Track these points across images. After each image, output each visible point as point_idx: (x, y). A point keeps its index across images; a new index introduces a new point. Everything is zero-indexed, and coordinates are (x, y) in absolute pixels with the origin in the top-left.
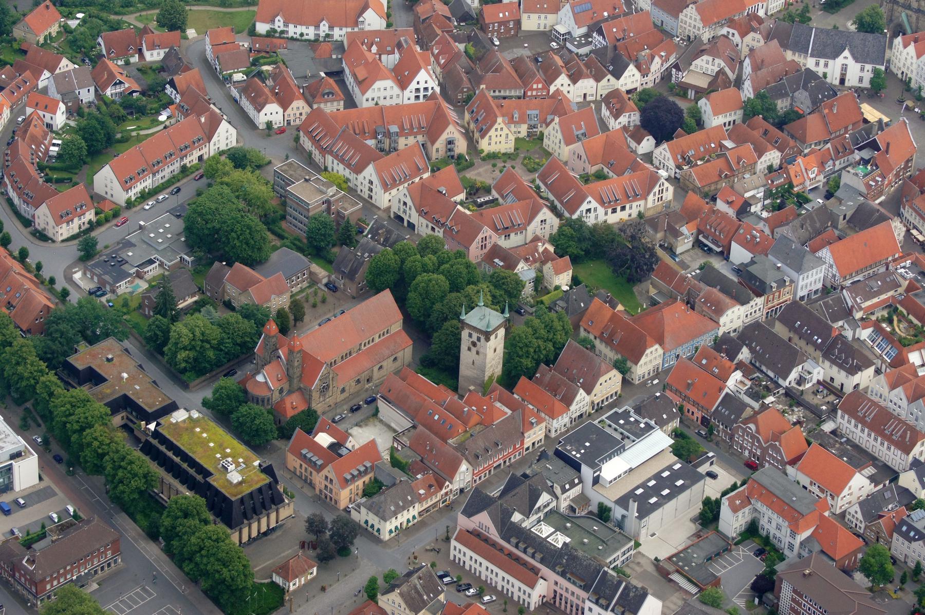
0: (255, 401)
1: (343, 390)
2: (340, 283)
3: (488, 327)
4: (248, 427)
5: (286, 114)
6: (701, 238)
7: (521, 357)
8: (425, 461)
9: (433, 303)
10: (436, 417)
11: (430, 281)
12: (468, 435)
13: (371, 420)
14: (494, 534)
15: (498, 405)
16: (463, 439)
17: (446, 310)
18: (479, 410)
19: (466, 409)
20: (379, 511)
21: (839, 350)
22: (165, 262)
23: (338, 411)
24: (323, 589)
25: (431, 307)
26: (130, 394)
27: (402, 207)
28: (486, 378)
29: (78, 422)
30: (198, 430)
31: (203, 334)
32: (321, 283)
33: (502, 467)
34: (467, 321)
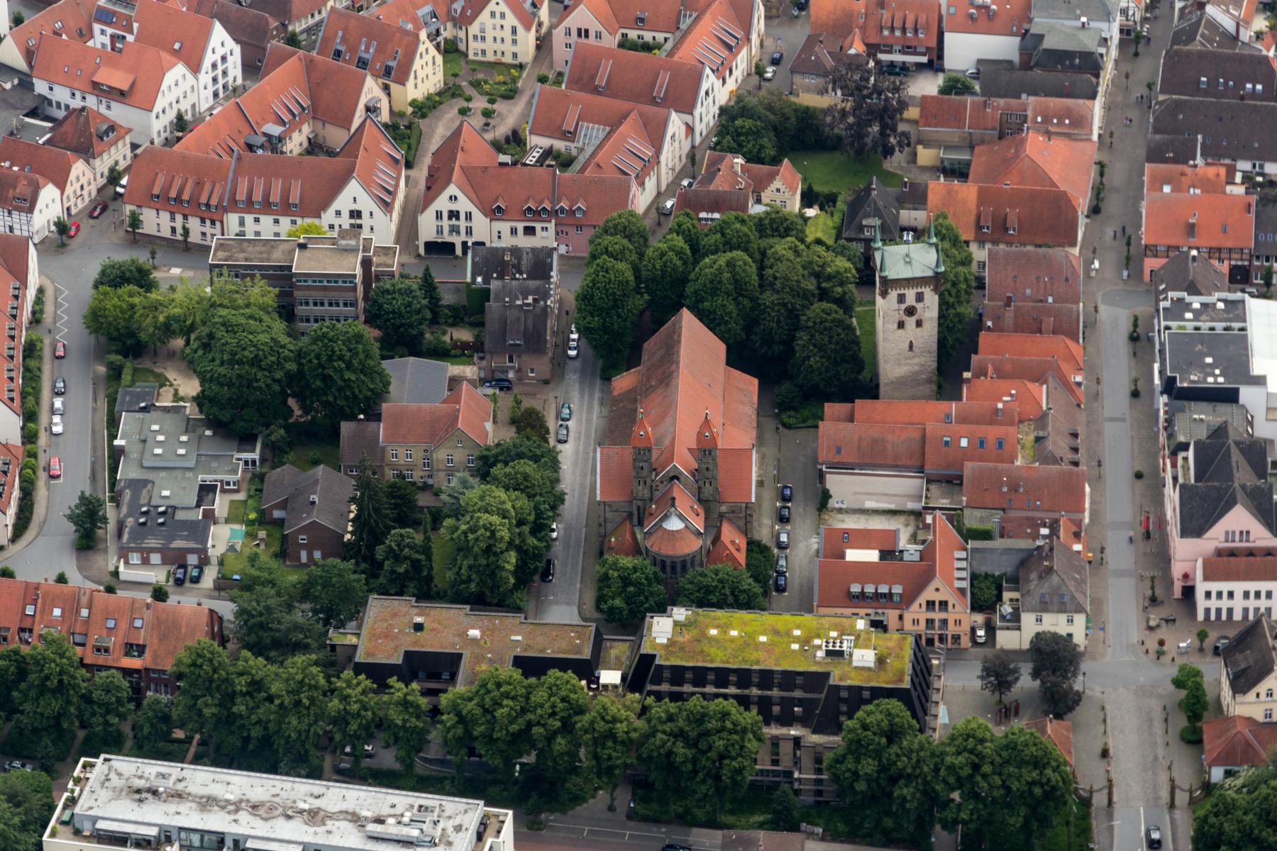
5: (64, 198)
7: (953, 306)
10: (964, 443)
17: (788, 298)
20: (1063, 603)
22: (226, 477)
24: (1105, 754)
26: (519, 651)
27: (446, 223)
29: (553, 714)
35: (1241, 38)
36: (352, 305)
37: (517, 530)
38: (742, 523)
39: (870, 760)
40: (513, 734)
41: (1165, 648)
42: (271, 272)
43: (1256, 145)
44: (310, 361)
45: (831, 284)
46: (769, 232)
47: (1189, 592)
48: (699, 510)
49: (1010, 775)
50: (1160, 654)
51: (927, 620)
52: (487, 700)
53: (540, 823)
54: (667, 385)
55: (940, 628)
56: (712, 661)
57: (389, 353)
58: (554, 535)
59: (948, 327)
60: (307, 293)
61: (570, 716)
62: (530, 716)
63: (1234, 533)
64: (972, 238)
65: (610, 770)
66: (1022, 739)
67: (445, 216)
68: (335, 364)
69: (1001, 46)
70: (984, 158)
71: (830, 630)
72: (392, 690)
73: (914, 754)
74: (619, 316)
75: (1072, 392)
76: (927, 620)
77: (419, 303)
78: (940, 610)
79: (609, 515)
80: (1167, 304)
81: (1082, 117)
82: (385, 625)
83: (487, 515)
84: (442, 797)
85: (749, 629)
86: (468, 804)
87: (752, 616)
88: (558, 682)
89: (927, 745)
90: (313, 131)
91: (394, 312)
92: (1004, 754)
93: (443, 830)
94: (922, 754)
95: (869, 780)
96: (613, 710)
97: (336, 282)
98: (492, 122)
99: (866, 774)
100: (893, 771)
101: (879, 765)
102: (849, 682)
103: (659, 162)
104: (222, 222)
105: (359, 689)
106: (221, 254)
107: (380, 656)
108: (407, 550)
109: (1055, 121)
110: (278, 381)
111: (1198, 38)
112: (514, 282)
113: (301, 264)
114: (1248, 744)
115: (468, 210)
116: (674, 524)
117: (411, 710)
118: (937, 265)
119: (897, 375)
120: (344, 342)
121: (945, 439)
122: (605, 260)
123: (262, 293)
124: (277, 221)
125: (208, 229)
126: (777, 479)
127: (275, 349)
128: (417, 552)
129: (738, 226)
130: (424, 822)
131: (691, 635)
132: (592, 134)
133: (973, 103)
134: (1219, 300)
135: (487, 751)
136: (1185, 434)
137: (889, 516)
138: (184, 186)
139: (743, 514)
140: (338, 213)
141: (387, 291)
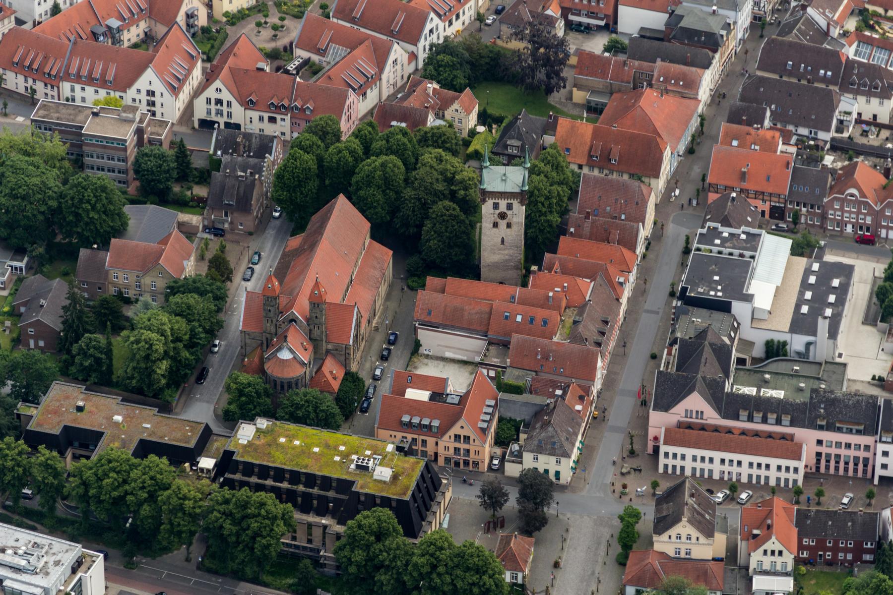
6: (571, 17)
7: (545, 214)
10: (519, 318)
14: (712, 417)
17: (422, 194)
20: (554, 449)
21: (857, 75)
24: (556, 565)
26: (145, 436)
27: (213, 107)
29: (143, 488)
35: (831, 34)
36: (123, 161)
37: (172, 345)
38: (343, 358)
39: (360, 551)
40: (114, 498)
41: (627, 490)
42: (74, 130)
43: (813, 117)
44: (67, 201)
45: (457, 188)
46: (430, 142)
47: (656, 450)
48: (307, 346)
49: (457, 576)
50: (623, 494)
51: (455, 449)
52: (100, 472)
53: (133, 564)
54: (312, 250)
55: (464, 455)
56: (274, 462)
57: (144, 199)
58: (216, 349)
59: (539, 228)
60: (92, 149)
61: (156, 491)
62: (127, 487)
63: (691, 411)
64: (584, 163)
65: (180, 533)
66: (469, 551)
67: (213, 102)
68: (84, 206)
69: (656, 20)
70: (615, 104)
71: (366, 449)
72: (39, 455)
73: (392, 551)
74: (302, 193)
75: (614, 289)
76: (455, 449)
77: (168, 165)
78: (464, 442)
79: (248, 341)
80: (704, 231)
81: (693, 81)
82: (58, 404)
83: (149, 332)
84: (53, 538)
85: (308, 441)
86: (70, 545)
87: (314, 431)
88: (151, 465)
89: (402, 546)
90: (149, 27)
91: (148, 171)
92: (455, 560)
93: (46, 563)
94: (398, 552)
95: (358, 566)
96: (185, 490)
97: (112, 143)
98: (279, 34)
99: (356, 561)
100: (376, 562)
101: (367, 556)
102: (366, 491)
103: (380, 79)
104: (58, 88)
105: (16, 451)
106: (41, 112)
107: (46, 426)
108: (92, 350)
109: (673, 82)
110: (43, 213)
111: (795, 31)
112: (239, 158)
113: (91, 128)
114: (655, 573)
115: (229, 100)
116: (285, 355)
117: (50, 471)
118: (523, 185)
119: (493, 261)
120: (92, 190)
121: (506, 314)
122: (295, 151)
123: (56, 146)
124: (97, 92)
125: (49, 90)
126: (390, 327)
127: (43, 189)
128: (101, 352)
129: (400, 136)
130: (33, 555)
131: (266, 440)
132: (336, 52)
133: (616, 61)
134: (744, 232)
135: (97, 508)
136: (682, 332)
137: (460, 365)
138: (35, 58)
139: (343, 352)
140: (139, 91)
141: (146, 155)
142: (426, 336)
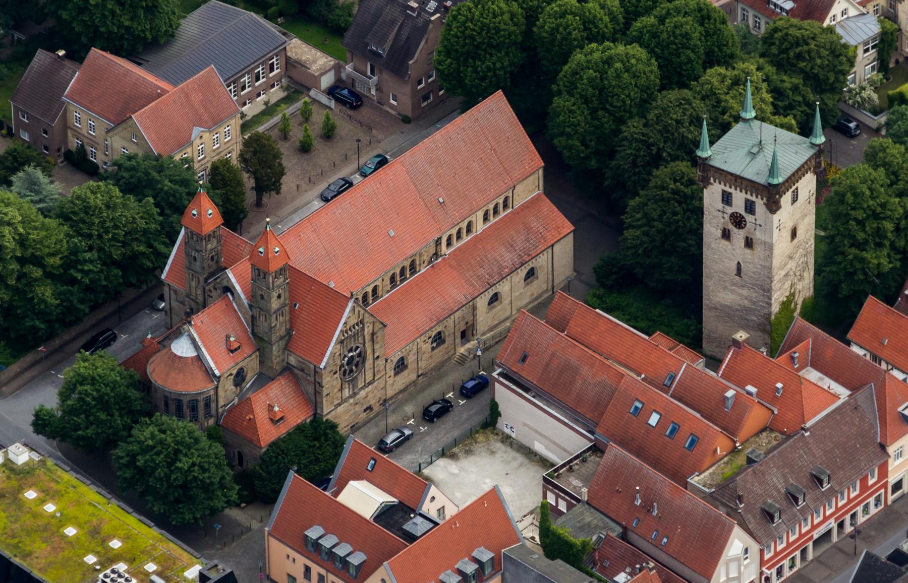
0: (173, 407)
1: (401, 366)
2: (369, 85)
3: (772, 172)
4: (160, 479)
8: (633, 537)
9: (621, 121)
10: (654, 419)
11: (608, 62)
12: (741, 460)
13: (480, 438)
15: (812, 375)
16: (728, 472)
18: (767, 395)
19: (730, 394)
23: (392, 419)
25: (617, 132)
28: (775, 308)
30: (31, 495)
31: (22, 241)
32: (318, 87)
33: (835, 538)
34: (717, 162)
142: (504, 395)
